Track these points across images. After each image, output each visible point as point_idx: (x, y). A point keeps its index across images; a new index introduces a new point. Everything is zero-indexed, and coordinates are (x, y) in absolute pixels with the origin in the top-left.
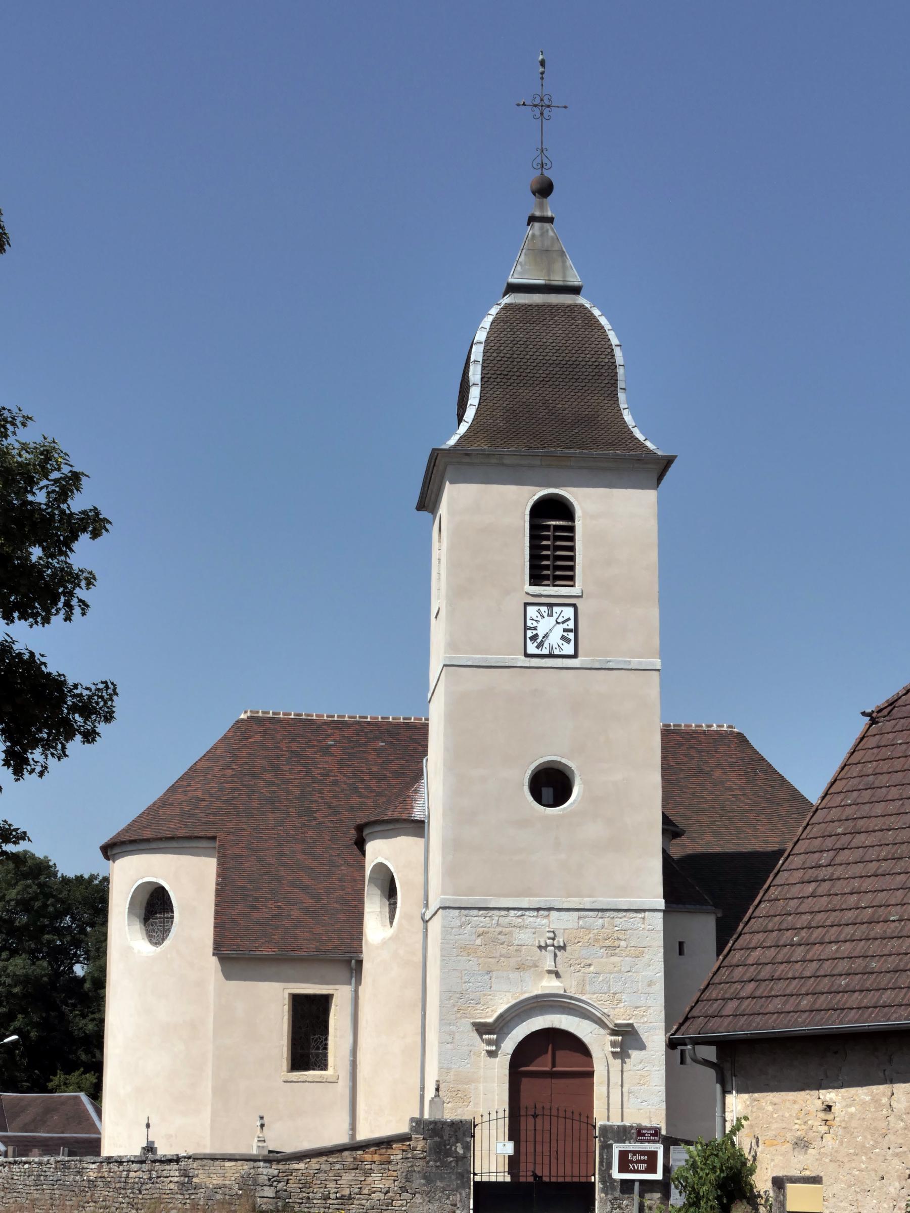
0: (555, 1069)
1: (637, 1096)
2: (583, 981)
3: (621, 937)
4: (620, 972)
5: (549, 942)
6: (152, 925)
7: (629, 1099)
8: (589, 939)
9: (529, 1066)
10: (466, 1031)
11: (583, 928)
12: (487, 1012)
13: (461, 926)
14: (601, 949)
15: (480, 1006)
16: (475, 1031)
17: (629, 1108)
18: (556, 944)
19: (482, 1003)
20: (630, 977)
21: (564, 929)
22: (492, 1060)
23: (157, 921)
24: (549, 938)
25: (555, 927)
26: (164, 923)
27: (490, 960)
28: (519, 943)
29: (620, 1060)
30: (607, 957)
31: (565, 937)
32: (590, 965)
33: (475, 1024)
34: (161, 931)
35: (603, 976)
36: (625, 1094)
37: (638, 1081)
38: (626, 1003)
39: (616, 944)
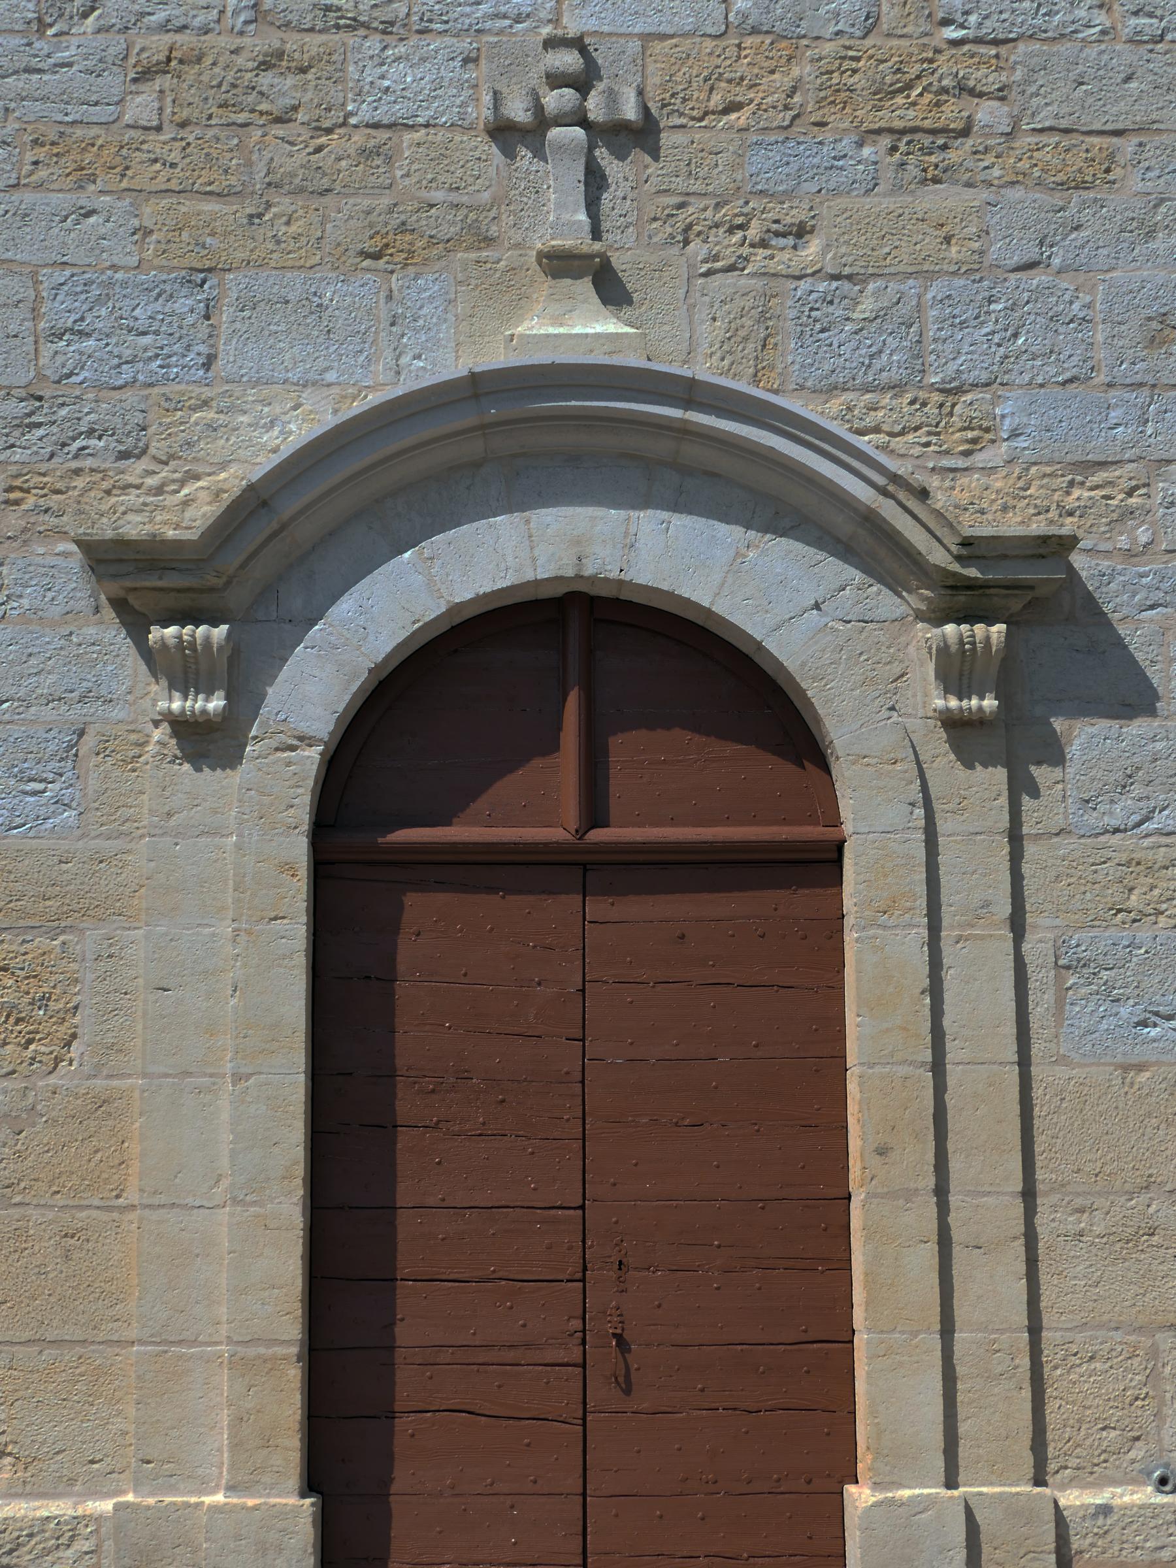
0: (597, 835)
1: (1109, 986)
2: (763, 317)
3: (979, 76)
4: (973, 269)
5: (557, 100)
7: (1060, 1003)
8: (794, 90)
9: (448, 823)
10: (55, 611)
11: (755, 31)
12: (186, 503)
13: (43, 26)
14: (860, 144)
15: (144, 464)
16: (109, 613)
17: (1062, 1060)
18: (595, 106)
19: (157, 447)
20: (1037, 294)
21: (647, 38)
22: (210, 777)
24: (556, 80)
25: (591, 25)
27: (210, 206)
28: (380, 115)
29: (1000, 774)
30: (898, 188)
31: (654, 80)
32: (801, 232)
33: (88, 547)
35: (876, 294)
36: (1040, 977)
37: (1114, 894)
38: (1021, 443)
39: (951, 113)
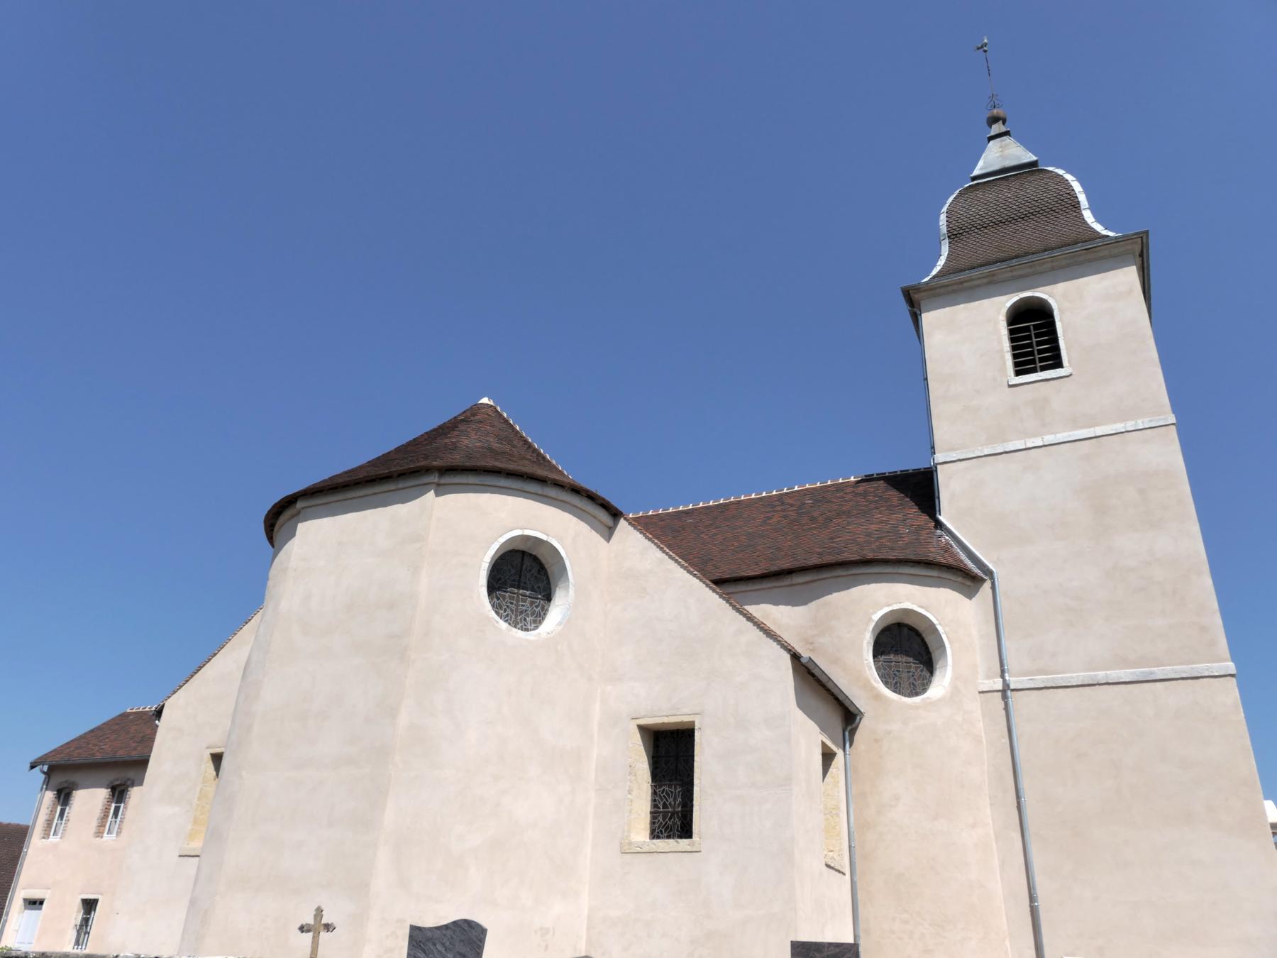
6: (498, 599)
23: (507, 594)
26: (518, 601)
34: (512, 611)
